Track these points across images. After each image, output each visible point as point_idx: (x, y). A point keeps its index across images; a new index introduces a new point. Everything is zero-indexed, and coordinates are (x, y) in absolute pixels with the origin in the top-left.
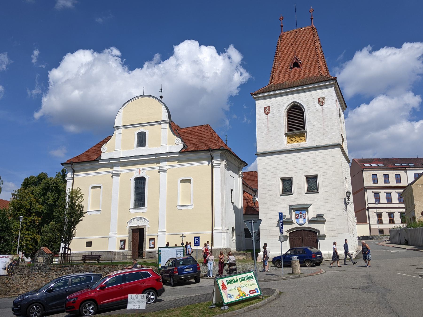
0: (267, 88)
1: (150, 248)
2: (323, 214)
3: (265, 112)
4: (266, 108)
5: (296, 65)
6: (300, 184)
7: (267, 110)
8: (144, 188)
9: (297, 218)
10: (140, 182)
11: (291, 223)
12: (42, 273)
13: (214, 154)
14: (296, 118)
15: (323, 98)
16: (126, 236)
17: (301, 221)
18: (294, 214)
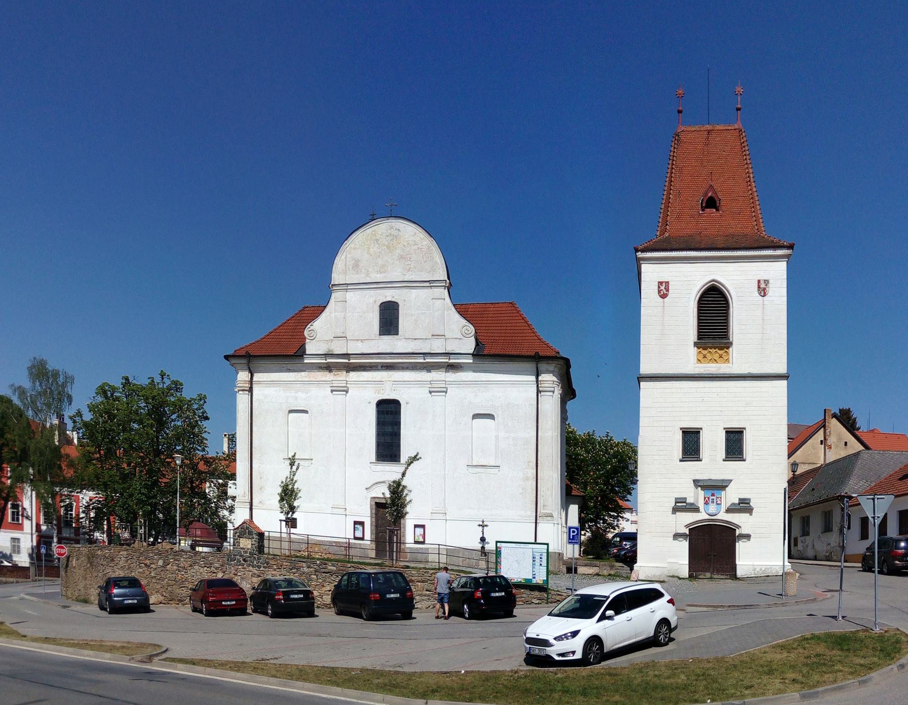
0: (659, 241)
1: (416, 542)
2: (749, 500)
3: (659, 292)
4: (660, 283)
5: (711, 203)
6: (713, 443)
7: (663, 288)
8: (397, 424)
9: (706, 503)
10: (388, 413)
11: (696, 510)
12: (251, 568)
13: (543, 366)
14: (714, 309)
15: (767, 282)
16: (366, 515)
17: (712, 508)
18: (701, 493)
